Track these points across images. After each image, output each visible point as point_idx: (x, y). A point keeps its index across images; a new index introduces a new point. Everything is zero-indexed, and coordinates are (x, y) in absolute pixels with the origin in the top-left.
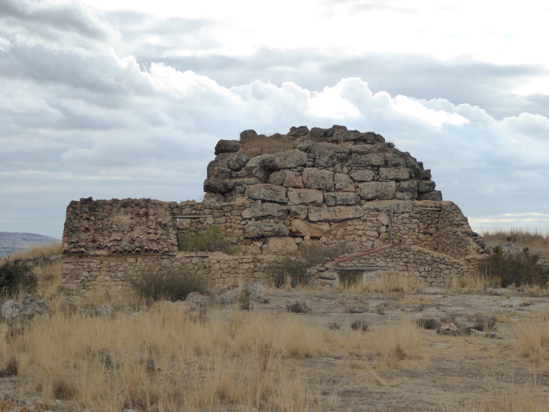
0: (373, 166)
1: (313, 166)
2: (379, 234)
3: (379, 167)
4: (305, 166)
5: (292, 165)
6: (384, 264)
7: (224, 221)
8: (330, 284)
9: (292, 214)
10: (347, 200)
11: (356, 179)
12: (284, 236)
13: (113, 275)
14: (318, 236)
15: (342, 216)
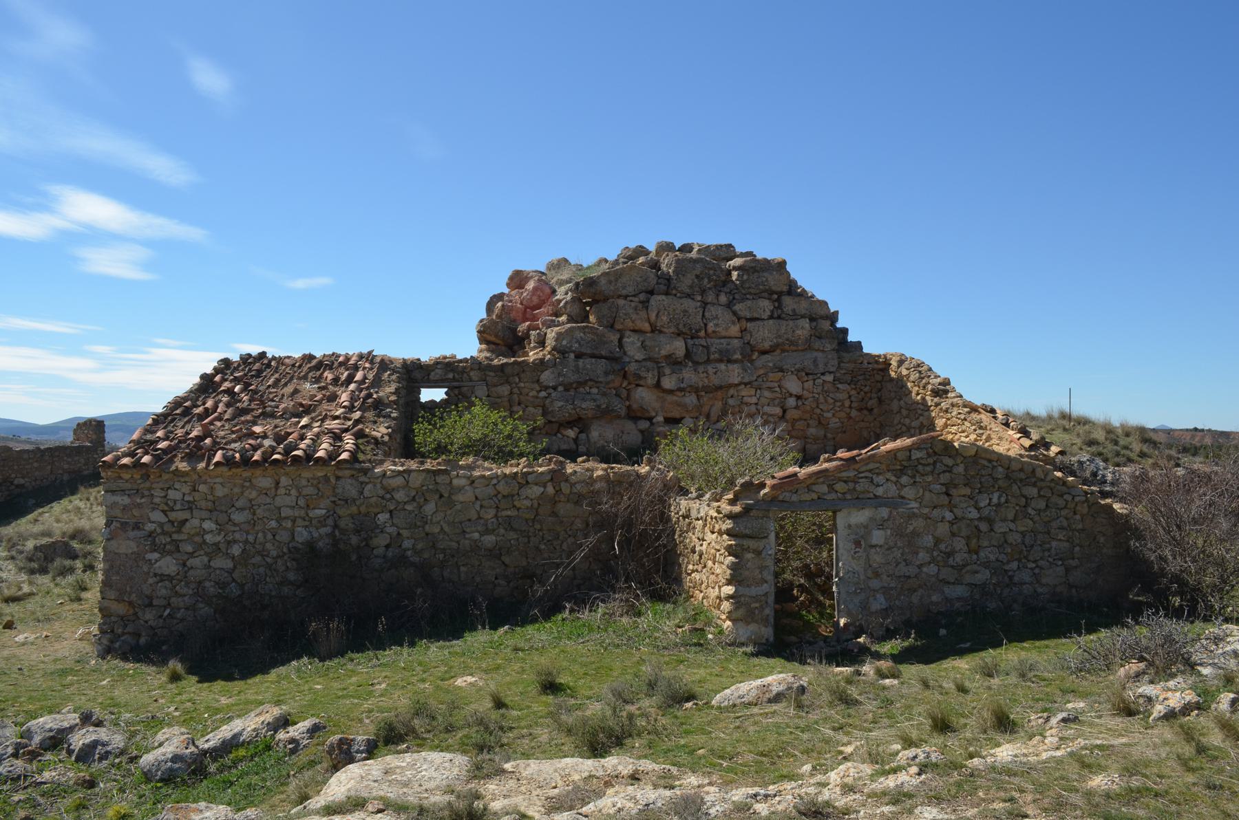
0: (772, 292)
1: (667, 294)
2: (784, 411)
3: (780, 294)
4: (651, 293)
5: (630, 290)
6: (892, 490)
7: (506, 393)
8: (754, 551)
9: (631, 379)
10: (728, 351)
11: (742, 314)
12: (619, 417)
13: (223, 518)
14: (678, 416)
15: (716, 381)
